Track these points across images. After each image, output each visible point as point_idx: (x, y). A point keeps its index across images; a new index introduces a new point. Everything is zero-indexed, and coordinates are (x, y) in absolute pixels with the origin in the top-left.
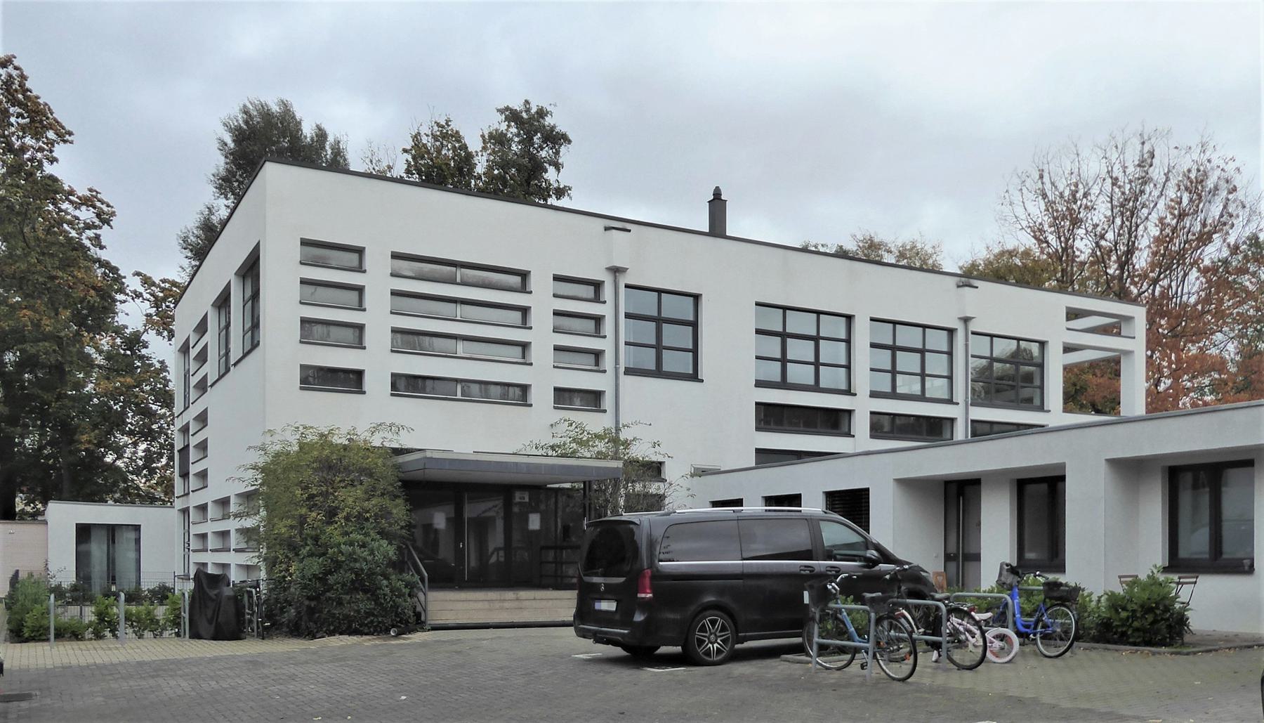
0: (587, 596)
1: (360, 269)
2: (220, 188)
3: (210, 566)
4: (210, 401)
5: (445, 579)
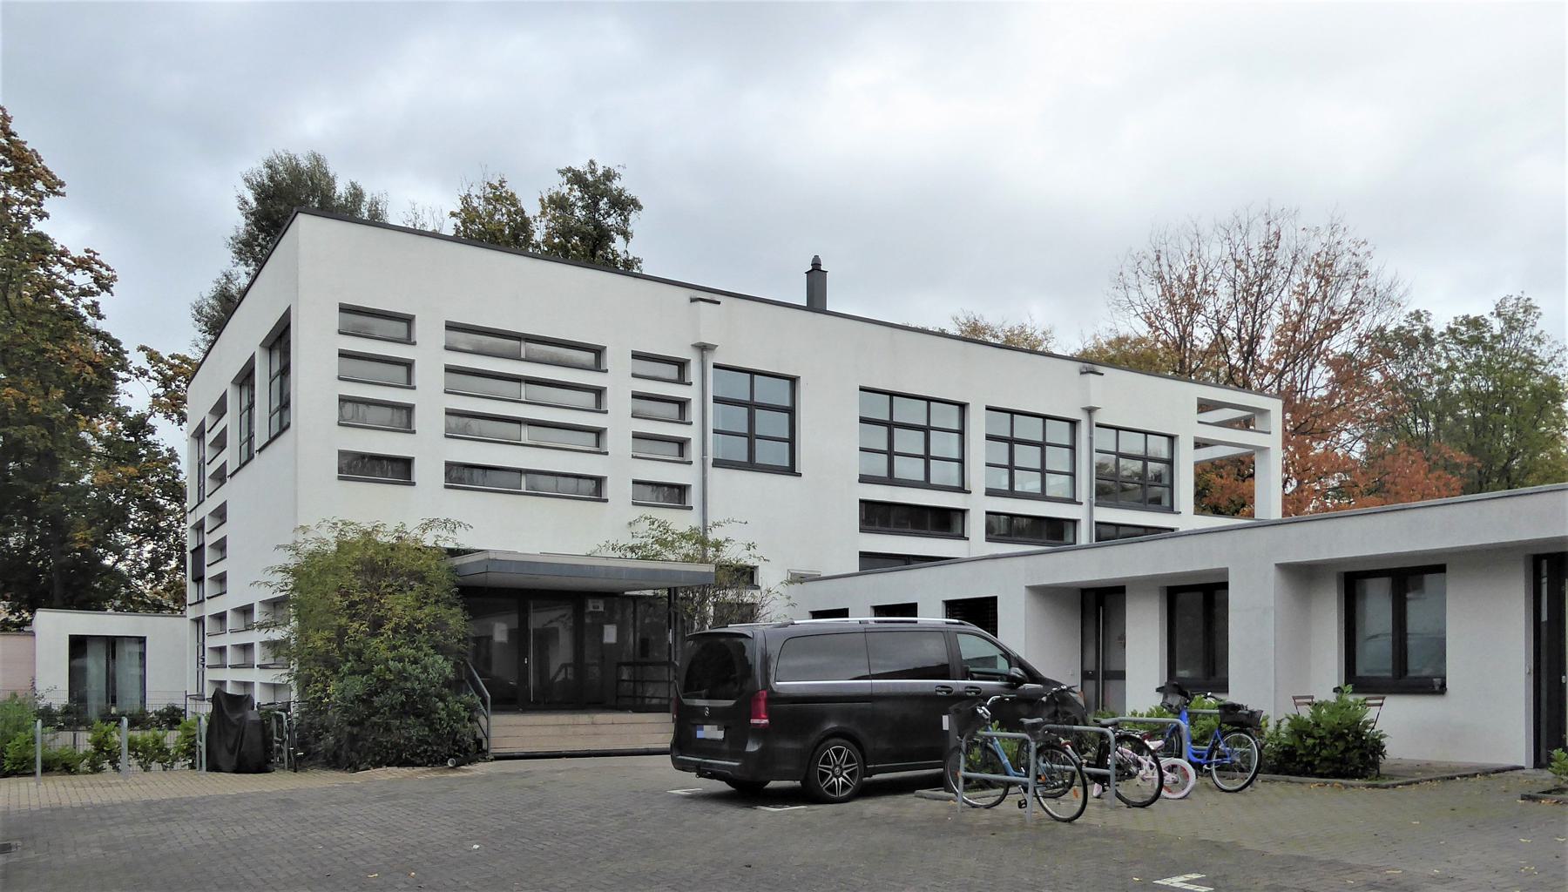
0: (686, 722)
1: (409, 340)
2: (239, 253)
3: (229, 685)
4: (229, 493)
5: (510, 700)
